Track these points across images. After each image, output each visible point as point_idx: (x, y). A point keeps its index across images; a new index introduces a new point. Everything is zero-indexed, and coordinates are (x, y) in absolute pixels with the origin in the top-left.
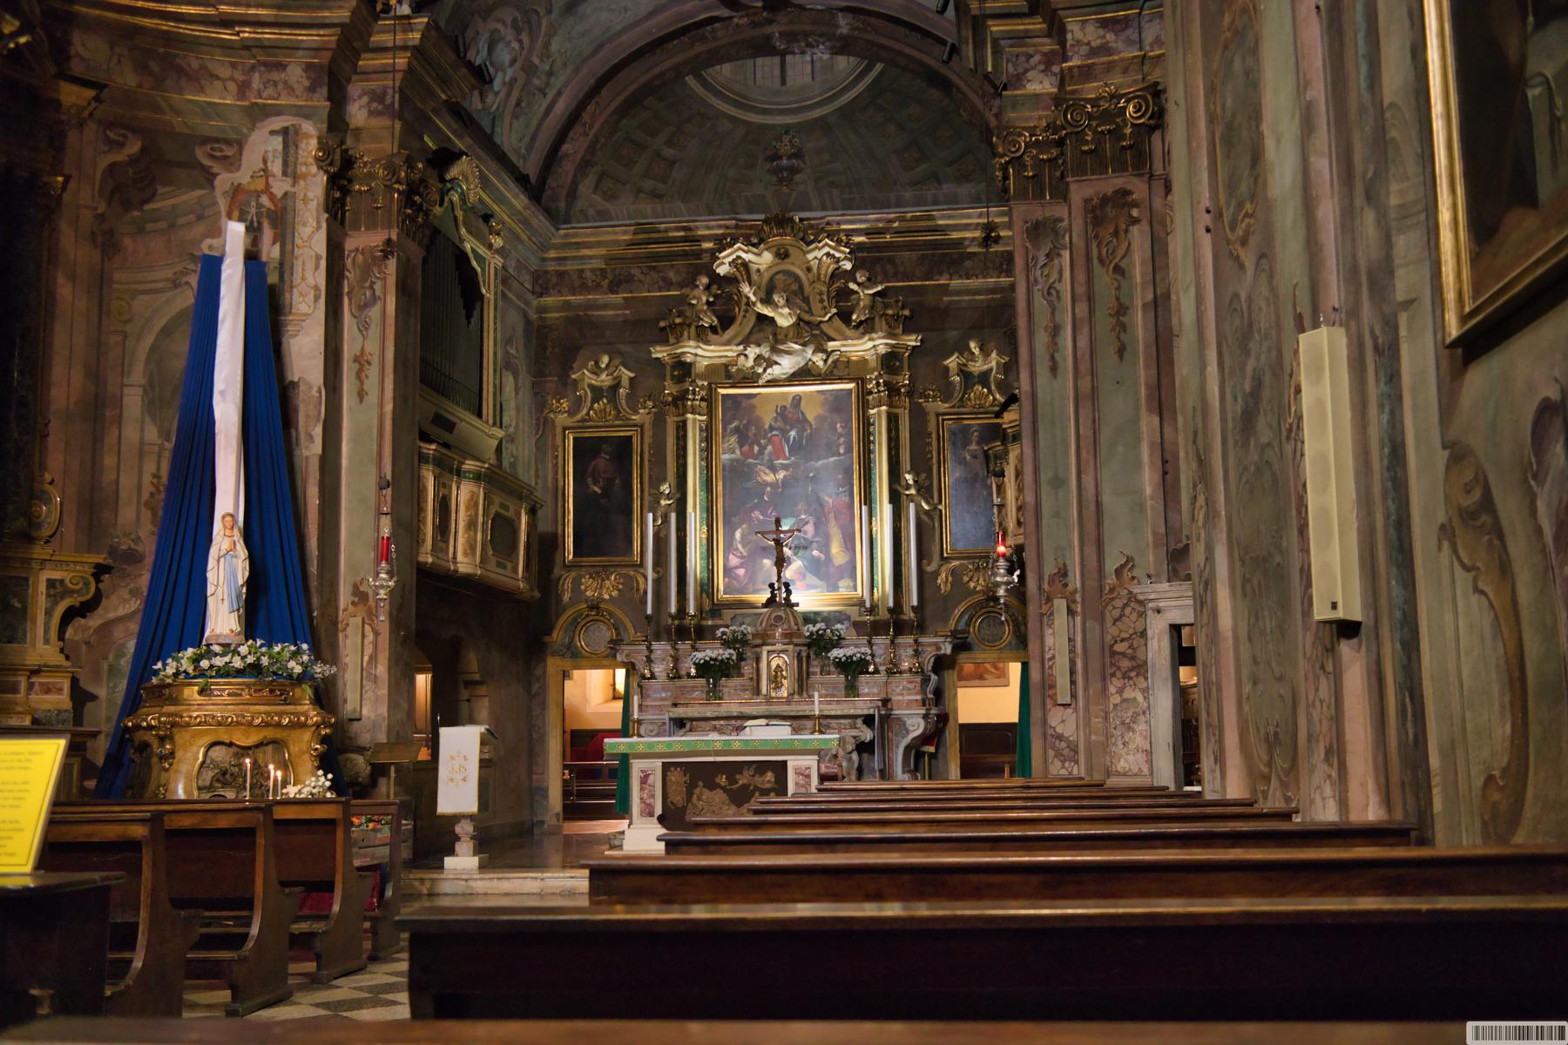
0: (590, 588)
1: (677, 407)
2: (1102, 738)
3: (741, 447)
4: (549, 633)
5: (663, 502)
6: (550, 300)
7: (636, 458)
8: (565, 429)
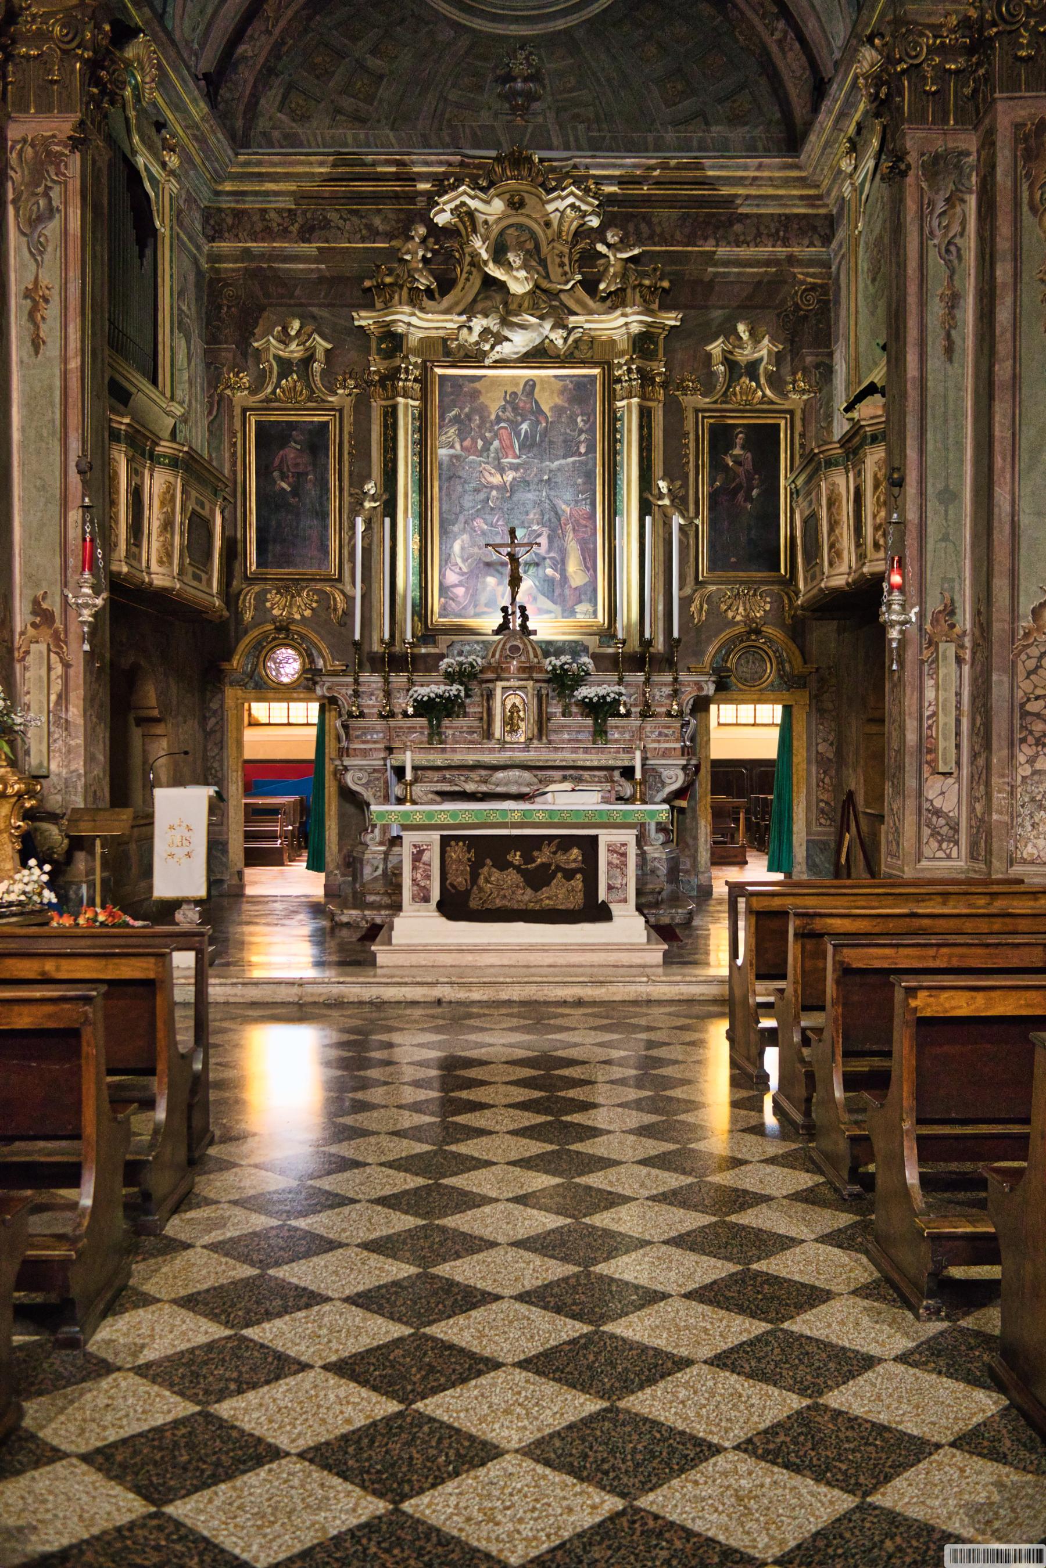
0: (278, 607)
1: (384, 387)
2: (1006, 818)
3: (462, 441)
4: (228, 658)
5: (367, 505)
6: (224, 246)
7: (333, 450)
8: (244, 410)
